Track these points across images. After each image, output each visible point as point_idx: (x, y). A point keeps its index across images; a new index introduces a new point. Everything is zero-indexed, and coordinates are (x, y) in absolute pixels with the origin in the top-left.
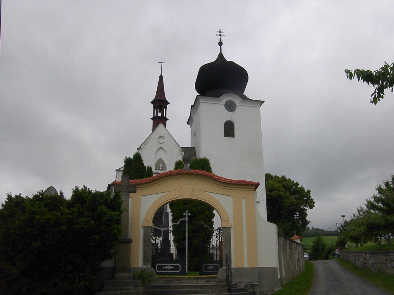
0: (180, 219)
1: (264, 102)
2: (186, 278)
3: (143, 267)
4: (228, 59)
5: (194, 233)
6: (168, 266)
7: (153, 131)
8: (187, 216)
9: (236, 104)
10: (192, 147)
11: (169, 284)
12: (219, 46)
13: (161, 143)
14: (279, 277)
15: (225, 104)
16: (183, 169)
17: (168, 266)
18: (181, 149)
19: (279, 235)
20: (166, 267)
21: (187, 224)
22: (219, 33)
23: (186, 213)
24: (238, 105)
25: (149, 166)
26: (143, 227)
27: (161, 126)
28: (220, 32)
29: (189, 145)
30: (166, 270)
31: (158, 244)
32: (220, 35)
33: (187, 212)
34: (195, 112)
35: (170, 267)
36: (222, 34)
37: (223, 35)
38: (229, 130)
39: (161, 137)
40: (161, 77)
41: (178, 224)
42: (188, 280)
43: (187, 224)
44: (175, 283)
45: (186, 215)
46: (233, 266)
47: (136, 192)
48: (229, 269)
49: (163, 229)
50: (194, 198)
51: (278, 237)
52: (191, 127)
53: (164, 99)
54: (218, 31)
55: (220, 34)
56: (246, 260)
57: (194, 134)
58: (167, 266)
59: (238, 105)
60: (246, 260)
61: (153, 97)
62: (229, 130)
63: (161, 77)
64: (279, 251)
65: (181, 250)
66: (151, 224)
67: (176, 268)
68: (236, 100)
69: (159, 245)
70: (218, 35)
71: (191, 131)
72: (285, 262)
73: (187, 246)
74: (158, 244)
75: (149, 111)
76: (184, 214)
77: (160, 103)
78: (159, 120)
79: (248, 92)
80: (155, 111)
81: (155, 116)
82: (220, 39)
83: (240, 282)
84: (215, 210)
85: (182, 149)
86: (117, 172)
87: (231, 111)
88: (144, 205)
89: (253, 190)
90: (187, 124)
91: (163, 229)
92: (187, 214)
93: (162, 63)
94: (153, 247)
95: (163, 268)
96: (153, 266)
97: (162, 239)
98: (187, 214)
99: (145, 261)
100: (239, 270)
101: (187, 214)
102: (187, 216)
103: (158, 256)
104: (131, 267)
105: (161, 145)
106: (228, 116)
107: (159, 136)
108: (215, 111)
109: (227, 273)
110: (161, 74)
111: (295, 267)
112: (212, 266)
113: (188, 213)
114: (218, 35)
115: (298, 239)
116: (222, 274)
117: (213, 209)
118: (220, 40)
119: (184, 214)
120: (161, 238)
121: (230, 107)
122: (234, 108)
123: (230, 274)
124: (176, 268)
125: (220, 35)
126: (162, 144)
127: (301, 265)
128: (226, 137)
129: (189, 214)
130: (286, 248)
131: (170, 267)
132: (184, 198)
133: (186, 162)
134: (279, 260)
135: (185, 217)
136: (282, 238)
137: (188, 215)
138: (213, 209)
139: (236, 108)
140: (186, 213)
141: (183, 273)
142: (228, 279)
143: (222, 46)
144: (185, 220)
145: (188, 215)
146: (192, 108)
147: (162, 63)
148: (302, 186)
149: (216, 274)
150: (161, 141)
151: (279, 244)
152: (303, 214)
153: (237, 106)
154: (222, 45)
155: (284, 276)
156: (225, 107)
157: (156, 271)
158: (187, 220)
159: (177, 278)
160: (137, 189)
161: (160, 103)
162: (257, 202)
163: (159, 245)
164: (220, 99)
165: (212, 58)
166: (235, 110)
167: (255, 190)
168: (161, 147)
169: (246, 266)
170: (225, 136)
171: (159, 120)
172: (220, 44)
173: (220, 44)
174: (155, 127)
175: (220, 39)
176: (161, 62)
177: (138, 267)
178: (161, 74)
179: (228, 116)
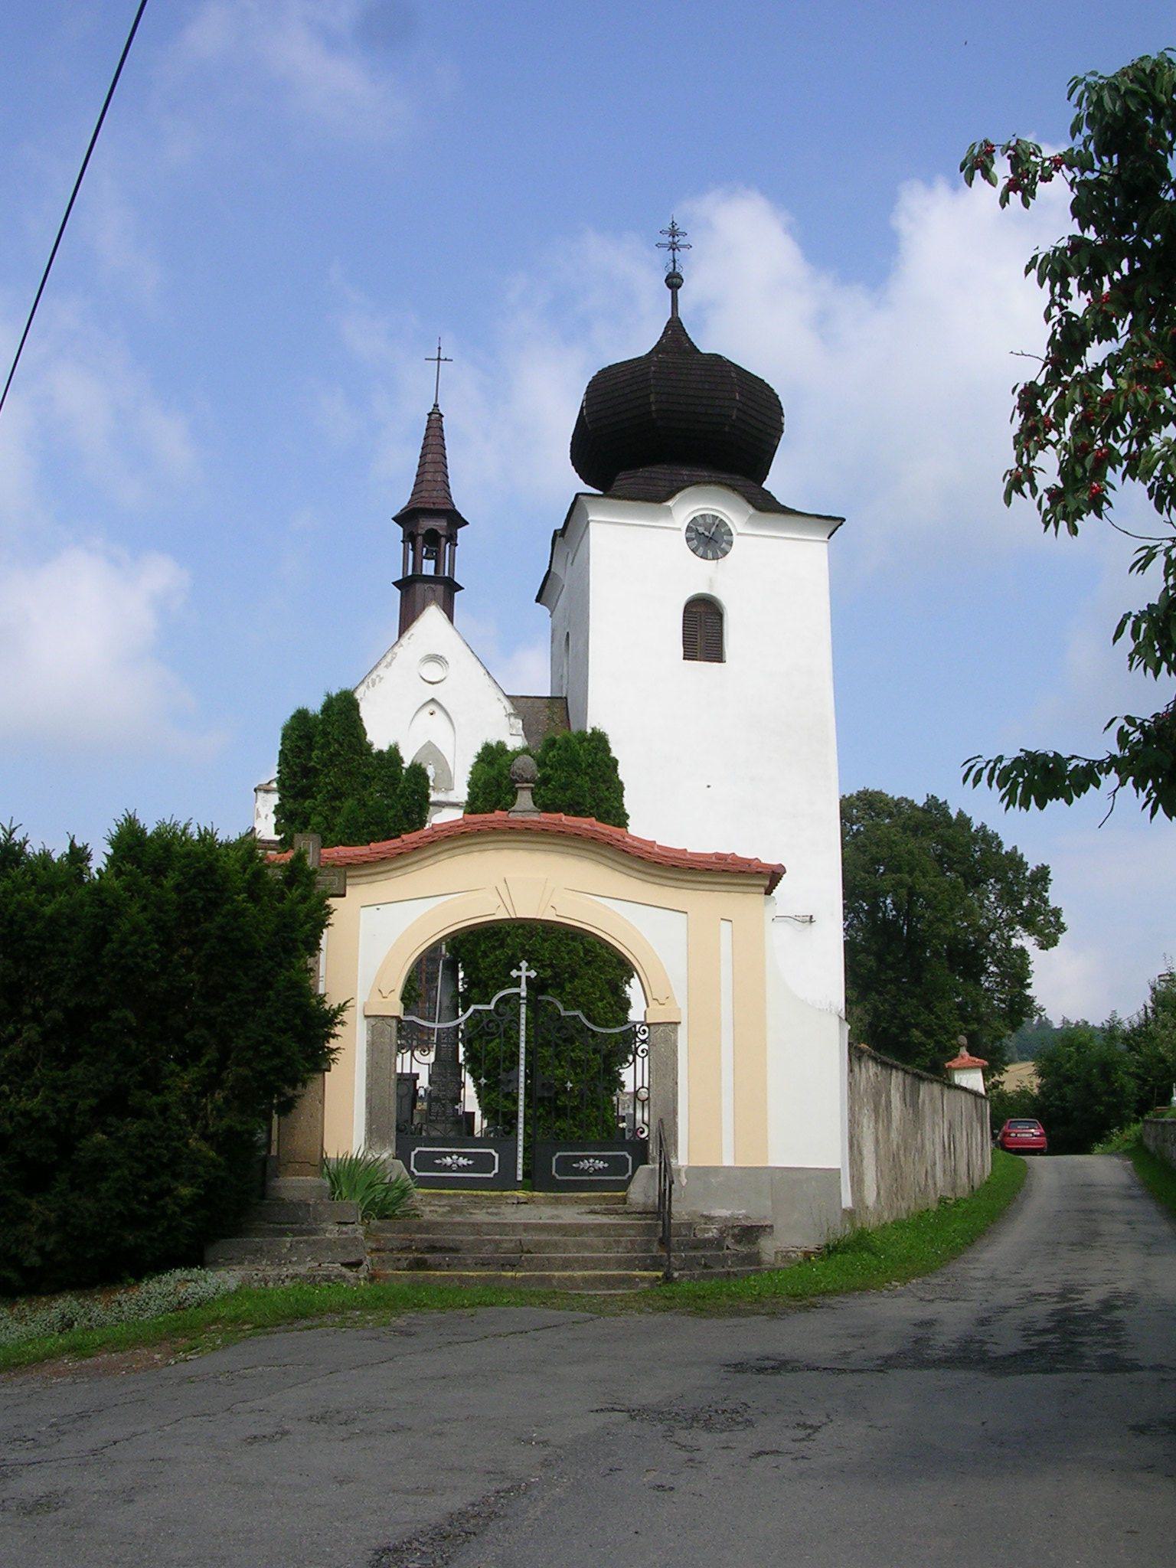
0: (502, 988)
4: (707, 343)
5: (553, 1036)
6: (455, 1159)
7: (400, 636)
8: (523, 980)
11: (458, 1219)
12: (670, 291)
14: (847, 1202)
15: (689, 529)
18: (506, 703)
19: (855, 1054)
20: (448, 1161)
23: (519, 969)
26: (367, 1017)
27: (432, 616)
28: (673, 233)
30: (584, 1172)
31: (417, 1076)
32: (674, 247)
34: (570, 557)
35: (463, 1161)
36: (681, 240)
37: (684, 246)
38: (703, 629)
40: (435, 423)
41: (492, 1007)
42: (523, 1206)
44: (480, 1216)
45: (519, 977)
47: (344, 895)
48: (666, 1172)
49: (436, 1025)
51: (850, 1060)
53: (449, 507)
54: (668, 226)
58: (450, 1154)
62: (703, 629)
63: (435, 423)
64: (851, 1109)
65: (500, 1115)
66: (396, 1008)
68: (733, 514)
69: (423, 1082)
71: (553, 631)
72: (882, 1152)
74: (417, 1076)
75: (390, 555)
76: (514, 973)
77: (430, 520)
80: (411, 553)
81: (410, 573)
83: (709, 1219)
86: (261, 795)
87: (710, 555)
88: (375, 937)
89: (763, 890)
90: (537, 601)
91: (436, 1025)
92: (524, 974)
94: (404, 1089)
96: (402, 1154)
97: (432, 1060)
98: (524, 972)
99: (373, 1132)
101: (524, 972)
102: (523, 980)
103: (410, 1119)
105: (431, 692)
106: (700, 576)
110: (436, 406)
111: (929, 1174)
112: (460, 1154)
115: (972, 1068)
116: (642, 1187)
119: (514, 973)
120: (431, 1057)
121: (709, 540)
122: (724, 545)
125: (674, 247)
127: (962, 1168)
128: (845, 816)
129: (533, 974)
130: (889, 1102)
131: (463, 1161)
134: (851, 1147)
135: (516, 982)
136: (871, 1064)
137: (528, 977)
139: (730, 544)
140: (519, 969)
141: (504, 1181)
144: (518, 994)
145: (528, 977)
146: (558, 539)
148: (1015, 848)
149: (624, 1185)
150: (433, 671)
151: (852, 1086)
152: (1017, 971)
153: (736, 539)
155: (870, 1198)
158: (524, 994)
159: (487, 1198)
160: (348, 881)
163: (423, 1082)
164: (669, 509)
165: (641, 340)
167: (768, 892)
168: (433, 700)
169: (728, 1161)
170: (689, 655)
172: (674, 282)
173: (674, 282)
178: (436, 406)
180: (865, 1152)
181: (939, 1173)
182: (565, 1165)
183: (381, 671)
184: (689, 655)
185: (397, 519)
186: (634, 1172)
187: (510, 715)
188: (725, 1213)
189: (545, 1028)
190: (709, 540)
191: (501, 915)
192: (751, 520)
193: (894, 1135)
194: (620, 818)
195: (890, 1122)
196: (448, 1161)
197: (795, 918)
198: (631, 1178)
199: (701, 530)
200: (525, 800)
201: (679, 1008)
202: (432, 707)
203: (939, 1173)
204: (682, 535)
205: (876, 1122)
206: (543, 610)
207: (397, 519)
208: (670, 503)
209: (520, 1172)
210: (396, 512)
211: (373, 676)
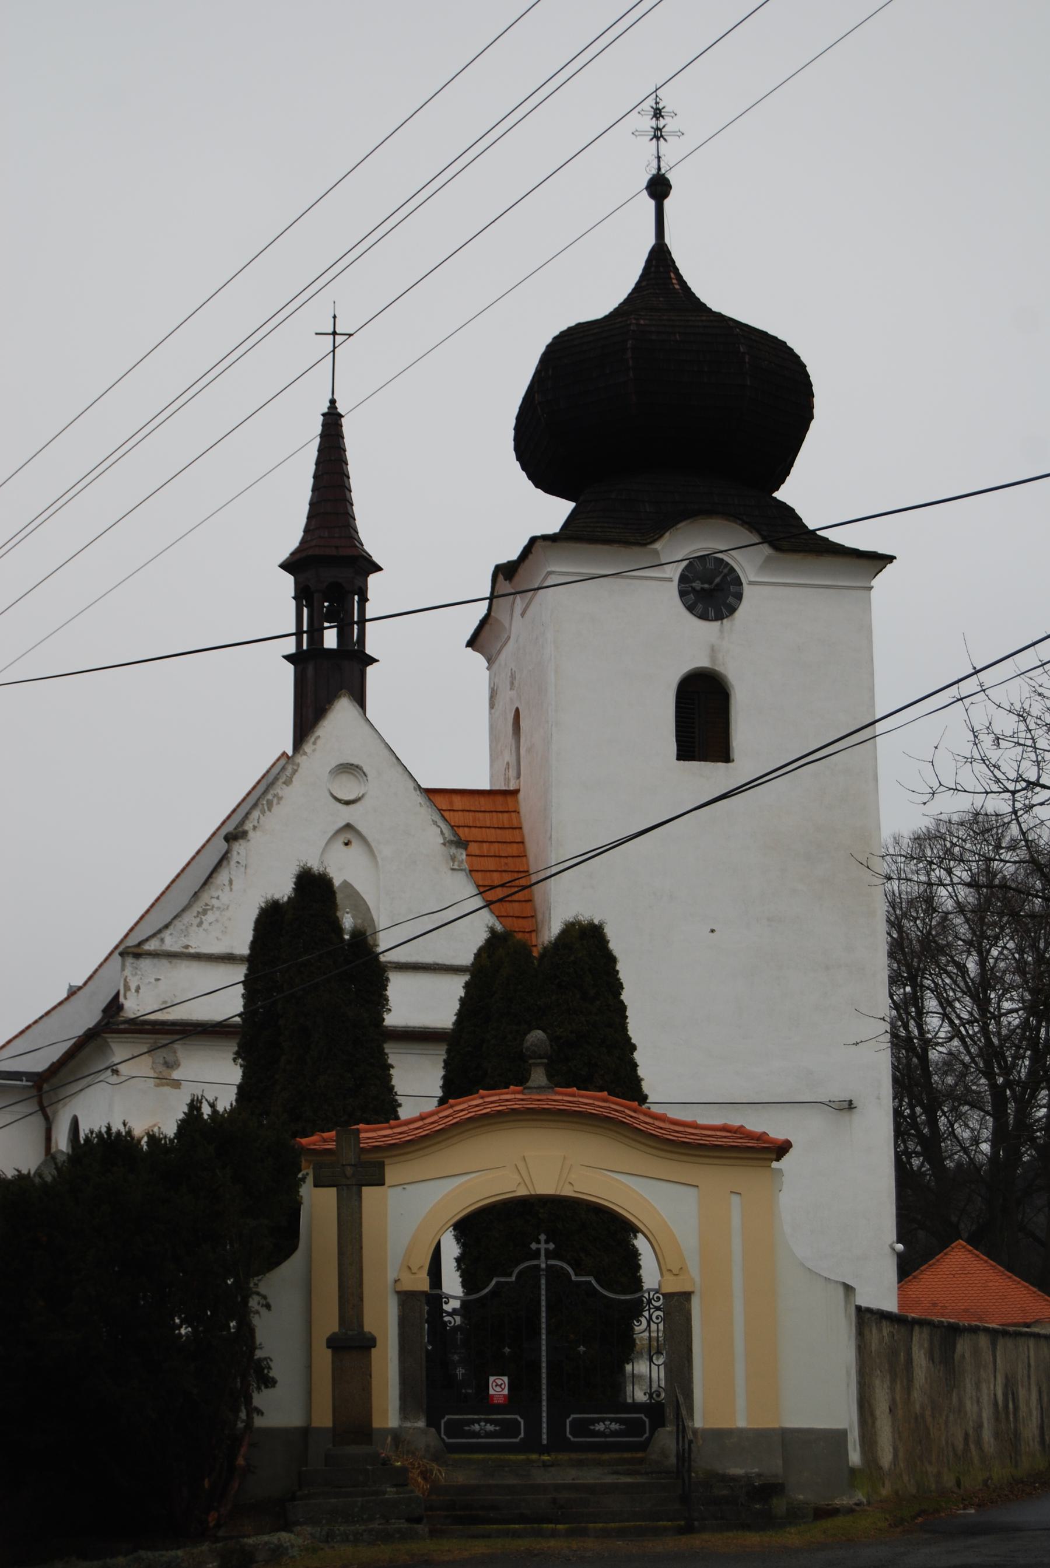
1: (890, 559)
2: (544, 1462)
3: (400, 1427)
8: (543, 1252)
9: (739, 577)
10: (496, 788)
13: (348, 803)
15: (683, 579)
16: (529, 1088)
17: (607, 1423)
20: (477, 1427)
21: (543, 1281)
22: (653, 123)
23: (538, 1242)
24: (751, 583)
25: (263, 905)
27: (343, 709)
29: (475, 774)
30: (476, 1435)
33: (543, 1237)
35: (490, 1428)
37: (673, 133)
38: (703, 716)
39: (349, 769)
41: (513, 1279)
43: (543, 1281)
45: (538, 1250)
46: (698, 1423)
48: (682, 1429)
50: (567, 1192)
52: (488, 669)
55: (658, 129)
56: (741, 1402)
57: (513, 726)
58: (478, 1421)
59: (751, 583)
60: (741, 1402)
61: (290, 534)
62: (703, 716)
63: (332, 424)
67: (509, 1429)
70: (642, 133)
73: (544, 1353)
76: (534, 1246)
77: (330, 568)
78: (329, 675)
79: (813, 488)
82: (659, 158)
84: (640, 1235)
85: (456, 834)
86: (130, 960)
87: (712, 614)
90: (471, 644)
93: (334, 333)
95: (467, 1428)
100: (719, 1435)
102: (543, 1252)
104: (376, 1424)
105: (346, 815)
106: (694, 643)
107: (334, 764)
108: (630, 626)
109: (678, 1444)
110: (333, 402)
112: (487, 1421)
113: (547, 1242)
114: (642, 133)
117: (635, 1230)
118: (655, 164)
121: (711, 593)
123: (686, 1446)
124: (509, 1429)
126: (352, 807)
130: (909, 1360)
131: (490, 1428)
132: (533, 1193)
133: (539, 1061)
135: (536, 1254)
137: (546, 1249)
138: (635, 1230)
139: (739, 597)
141: (531, 1444)
142: (684, 1457)
143: (667, 202)
144: (538, 1267)
146: (501, 577)
147: (334, 333)
149: (644, 1446)
150: (347, 789)
151: (862, 1348)
154: (666, 195)
155: (886, 1458)
156: (682, 594)
157: (443, 1440)
161: (330, 568)
162: (846, 1105)
166: (732, 610)
168: (348, 826)
169: (741, 1423)
171: (329, 675)
172: (659, 188)
173: (659, 188)
174: (308, 717)
175: (659, 158)
176: (331, 330)
177: (385, 1426)
178: (333, 402)
179: (694, 643)
180: (878, 1413)
181: (987, 1434)
182: (581, 1428)
183: (280, 789)
184: (681, 757)
185: (285, 566)
186: (652, 1433)
187: (451, 842)
188: (739, 1471)
189: (558, 1293)
190: (711, 593)
191: (522, 1192)
192: (767, 565)
193: (916, 1394)
194: (629, 1086)
195: (910, 1380)
196: (477, 1427)
197: (828, 1104)
198: (649, 1439)
199: (697, 585)
200: (538, 1077)
201: (694, 1278)
202: (349, 836)
203: (987, 1434)
204: (672, 589)
205: (893, 1381)
206: (478, 660)
207: (285, 566)
208: (657, 546)
209: (544, 1436)
210: (284, 555)
211: (269, 797)
